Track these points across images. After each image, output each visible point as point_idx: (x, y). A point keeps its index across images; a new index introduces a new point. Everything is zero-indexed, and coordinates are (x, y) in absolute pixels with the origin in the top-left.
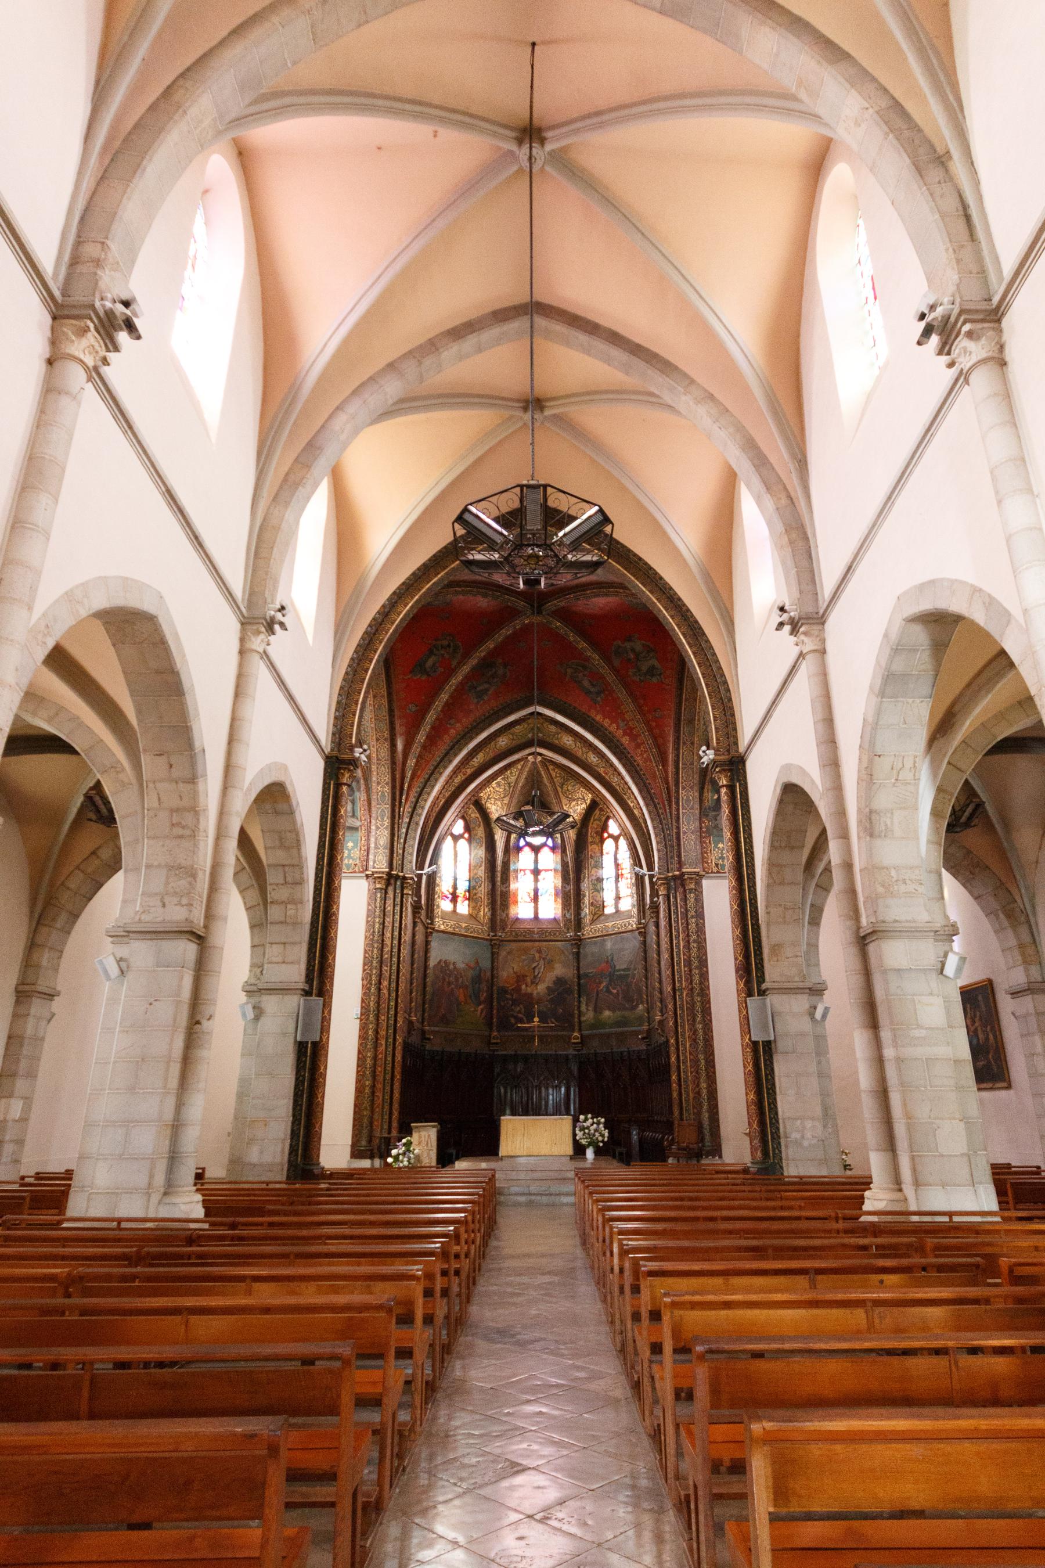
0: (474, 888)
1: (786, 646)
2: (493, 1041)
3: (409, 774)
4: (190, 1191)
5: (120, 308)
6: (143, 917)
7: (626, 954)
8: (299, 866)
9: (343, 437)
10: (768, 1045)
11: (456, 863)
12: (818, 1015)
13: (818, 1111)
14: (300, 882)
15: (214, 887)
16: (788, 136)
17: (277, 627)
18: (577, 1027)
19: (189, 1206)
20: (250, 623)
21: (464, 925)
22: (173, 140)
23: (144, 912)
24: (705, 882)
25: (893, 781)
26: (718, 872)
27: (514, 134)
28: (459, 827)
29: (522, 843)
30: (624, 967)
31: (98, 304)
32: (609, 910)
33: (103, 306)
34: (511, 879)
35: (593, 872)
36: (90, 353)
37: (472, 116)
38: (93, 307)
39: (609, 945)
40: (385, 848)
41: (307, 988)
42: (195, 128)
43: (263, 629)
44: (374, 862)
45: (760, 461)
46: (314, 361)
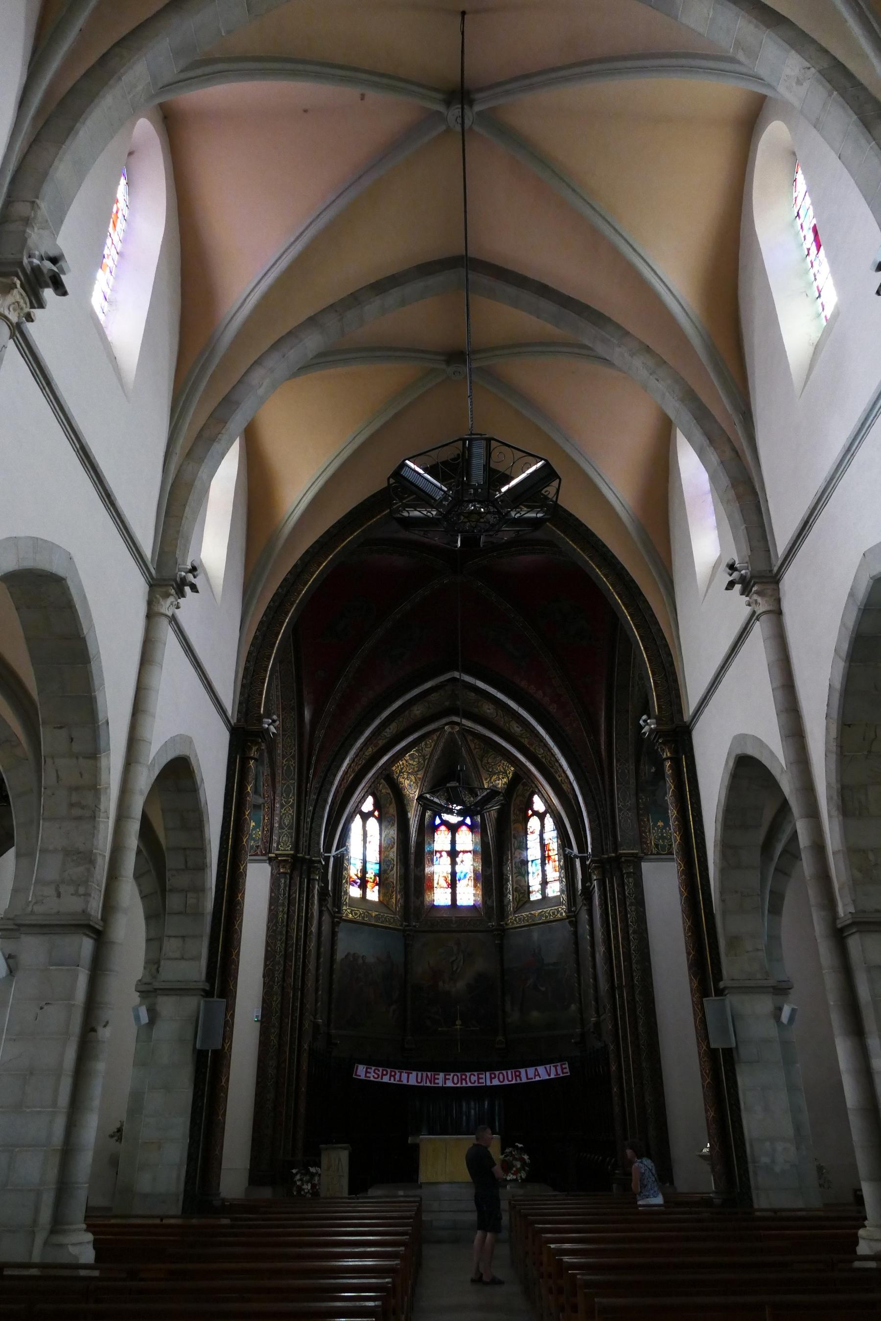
0: (385, 871)
1: (737, 606)
3: (317, 746)
4: (80, 1230)
5: (48, 265)
6: (36, 908)
8: (201, 849)
9: (261, 391)
10: (729, 1054)
11: (365, 843)
12: (785, 1018)
13: (790, 1132)
14: (202, 867)
15: (113, 875)
16: (720, 94)
17: (187, 589)
19: (81, 1248)
20: (160, 586)
21: (374, 914)
22: (109, 102)
23: (36, 903)
24: (645, 866)
25: (866, 753)
26: (658, 854)
27: (440, 96)
28: (368, 805)
29: (438, 821)
31: (25, 261)
32: (535, 896)
33: (31, 263)
34: (426, 862)
35: (517, 854)
36: (15, 310)
37: (401, 80)
38: (20, 264)
39: (535, 936)
40: (291, 828)
41: (208, 988)
42: (129, 93)
43: (173, 592)
44: (278, 844)
45: (702, 415)
46: (232, 318)
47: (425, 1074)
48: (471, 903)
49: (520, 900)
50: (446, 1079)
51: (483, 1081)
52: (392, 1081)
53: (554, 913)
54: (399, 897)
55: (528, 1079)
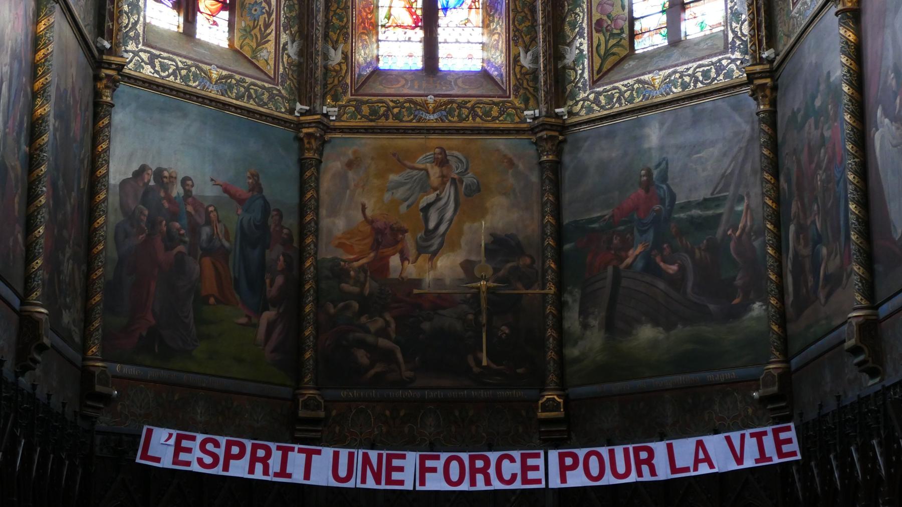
2: (302, 413)
7: (708, 159)
18: (552, 378)
30: (704, 193)
39: (654, 134)
47: (359, 454)
48: (477, 66)
49: (608, 54)
50: (424, 470)
51: (540, 474)
52: (258, 474)
53: (706, 74)
54: (284, 38)
55: (674, 469)
